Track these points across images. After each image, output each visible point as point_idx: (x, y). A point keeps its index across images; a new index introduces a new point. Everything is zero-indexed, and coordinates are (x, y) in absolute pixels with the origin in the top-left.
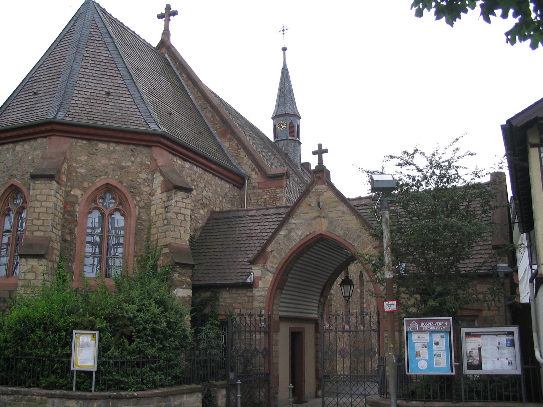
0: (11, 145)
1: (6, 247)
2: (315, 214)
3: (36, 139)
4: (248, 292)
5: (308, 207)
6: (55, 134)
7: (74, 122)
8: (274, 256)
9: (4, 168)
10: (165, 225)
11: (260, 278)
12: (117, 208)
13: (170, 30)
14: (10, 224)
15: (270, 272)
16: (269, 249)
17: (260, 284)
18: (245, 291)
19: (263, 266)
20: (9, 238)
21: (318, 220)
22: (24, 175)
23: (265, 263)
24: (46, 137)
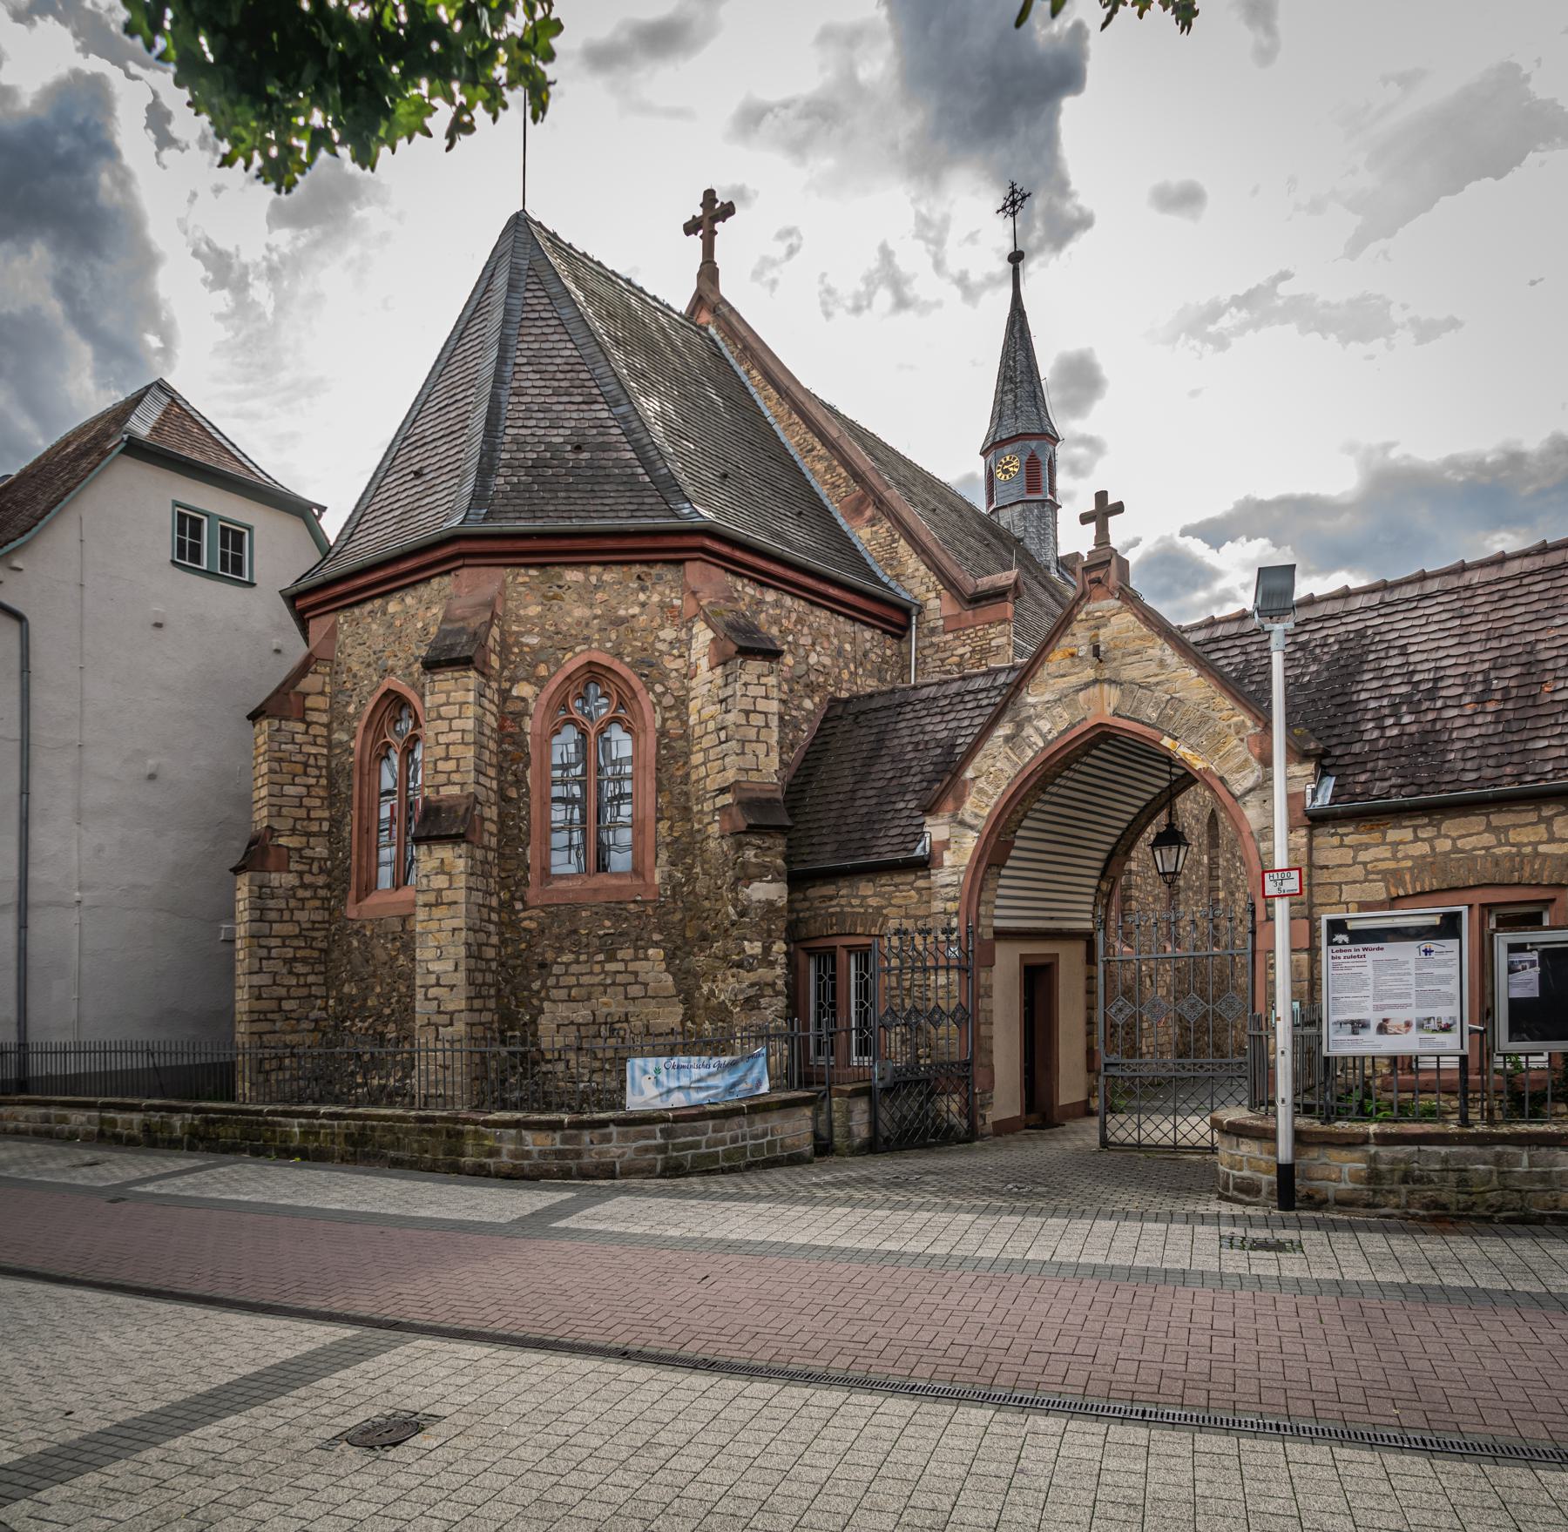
0: (378, 602)
2: (1090, 674)
5: (1068, 661)
8: (981, 791)
11: (945, 845)
16: (969, 774)
17: (948, 858)
23: (958, 808)
24: (448, 572)
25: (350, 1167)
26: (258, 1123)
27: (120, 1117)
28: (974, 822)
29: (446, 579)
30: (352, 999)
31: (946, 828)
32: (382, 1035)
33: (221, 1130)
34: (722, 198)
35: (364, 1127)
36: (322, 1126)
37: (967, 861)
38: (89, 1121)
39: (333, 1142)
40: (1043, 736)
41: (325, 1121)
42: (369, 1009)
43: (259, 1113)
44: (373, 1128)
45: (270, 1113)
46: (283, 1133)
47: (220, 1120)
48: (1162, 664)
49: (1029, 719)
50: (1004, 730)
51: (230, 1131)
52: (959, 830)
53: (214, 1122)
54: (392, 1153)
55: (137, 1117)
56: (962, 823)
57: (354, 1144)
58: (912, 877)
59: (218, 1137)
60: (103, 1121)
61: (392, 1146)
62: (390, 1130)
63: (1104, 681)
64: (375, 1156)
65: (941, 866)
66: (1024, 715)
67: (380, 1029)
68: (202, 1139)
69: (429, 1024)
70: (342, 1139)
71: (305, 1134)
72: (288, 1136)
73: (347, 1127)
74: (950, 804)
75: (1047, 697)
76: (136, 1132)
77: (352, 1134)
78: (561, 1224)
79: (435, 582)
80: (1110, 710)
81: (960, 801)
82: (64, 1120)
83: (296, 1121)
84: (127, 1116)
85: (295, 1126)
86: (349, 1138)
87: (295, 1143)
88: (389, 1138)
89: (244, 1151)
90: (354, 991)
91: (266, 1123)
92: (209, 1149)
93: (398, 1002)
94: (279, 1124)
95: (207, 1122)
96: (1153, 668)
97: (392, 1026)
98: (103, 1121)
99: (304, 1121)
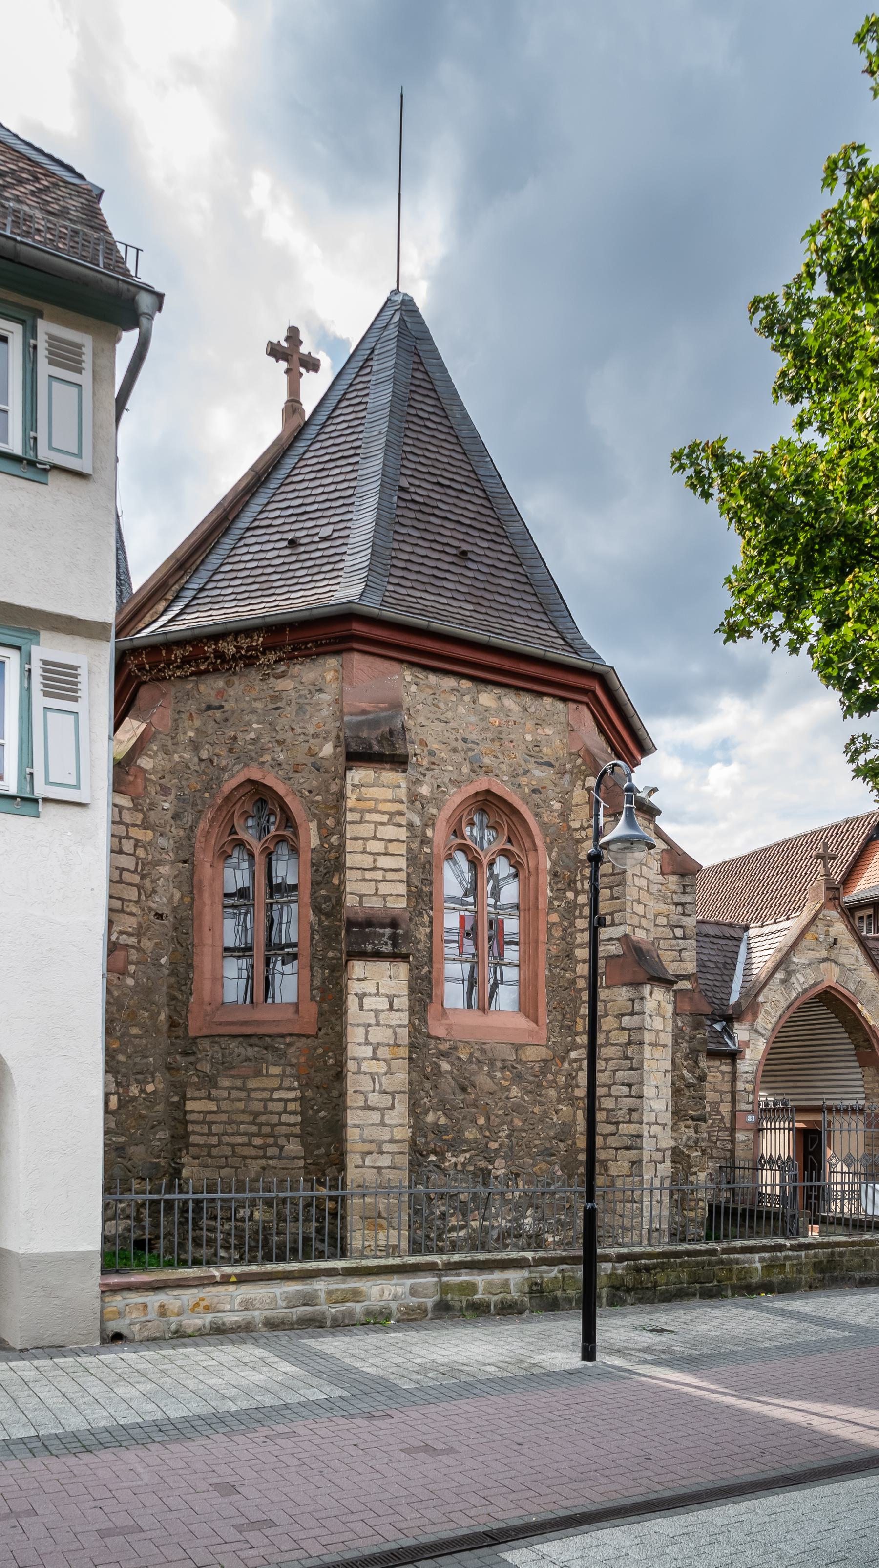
0: (466, 684)
1: (456, 938)
2: (824, 954)
3: (541, 695)
4: (722, 1064)
5: (814, 942)
6: (356, 646)
7: (315, 612)
8: (767, 1012)
9: (456, 740)
10: (675, 938)
11: (747, 1044)
12: (306, 856)
13: (302, 400)
14: (461, 884)
15: (762, 1036)
16: (761, 999)
17: (748, 1053)
18: (718, 1063)
19: (752, 1025)
20: (462, 918)
21: (827, 964)
22: (517, 775)
23: (754, 1021)
24: (564, 700)
25: (819, 1292)
26: (709, 1263)
27: (480, 1279)
28: (763, 1032)
29: (560, 705)
30: (438, 1130)
31: (747, 1032)
32: (486, 1173)
33: (661, 1277)
34: (280, 337)
35: (833, 1254)
36: (787, 1258)
37: (759, 1058)
38: (413, 1292)
39: (799, 1272)
40: (801, 985)
41: (790, 1253)
42: (466, 1141)
43: (713, 1252)
44: (841, 1254)
45: (725, 1251)
46: (740, 1271)
47: (655, 1267)
48: (857, 960)
49: (794, 971)
50: (780, 975)
51: (673, 1276)
52: (755, 1035)
53: (647, 1269)
54: (858, 1275)
55: (515, 1277)
56: (757, 1031)
57: (823, 1271)
58: (718, 1063)
59: (655, 1285)
60: (444, 1289)
61: (859, 1268)
62: (856, 1254)
63: (832, 960)
64: (843, 1279)
65: (744, 1058)
66: (791, 968)
67: (483, 1164)
68: (628, 1290)
69: (651, 1161)
70: (810, 1267)
71: (769, 1267)
72: (749, 1272)
73: (815, 1256)
74: (749, 1017)
75: (803, 961)
76: (515, 1295)
77: (821, 1262)
78: (846, 1334)
79: (547, 700)
80: (835, 979)
81: (755, 1015)
82: (356, 1295)
83: (756, 1256)
84: (497, 1276)
85: (756, 1262)
86: (818, 1266)
87: (756, 1279)
88: (857, 1261)
89: (694, 1295)
90: (442, 1121)
91: (721, 1262)
92: (641, 1300)
93: (509, 1136)
94: (737, 1262)
95: (638, 1270)
96: (853, 961)
97: (499, 1162)
98: (444, 1289)
99: (766, 1255)
